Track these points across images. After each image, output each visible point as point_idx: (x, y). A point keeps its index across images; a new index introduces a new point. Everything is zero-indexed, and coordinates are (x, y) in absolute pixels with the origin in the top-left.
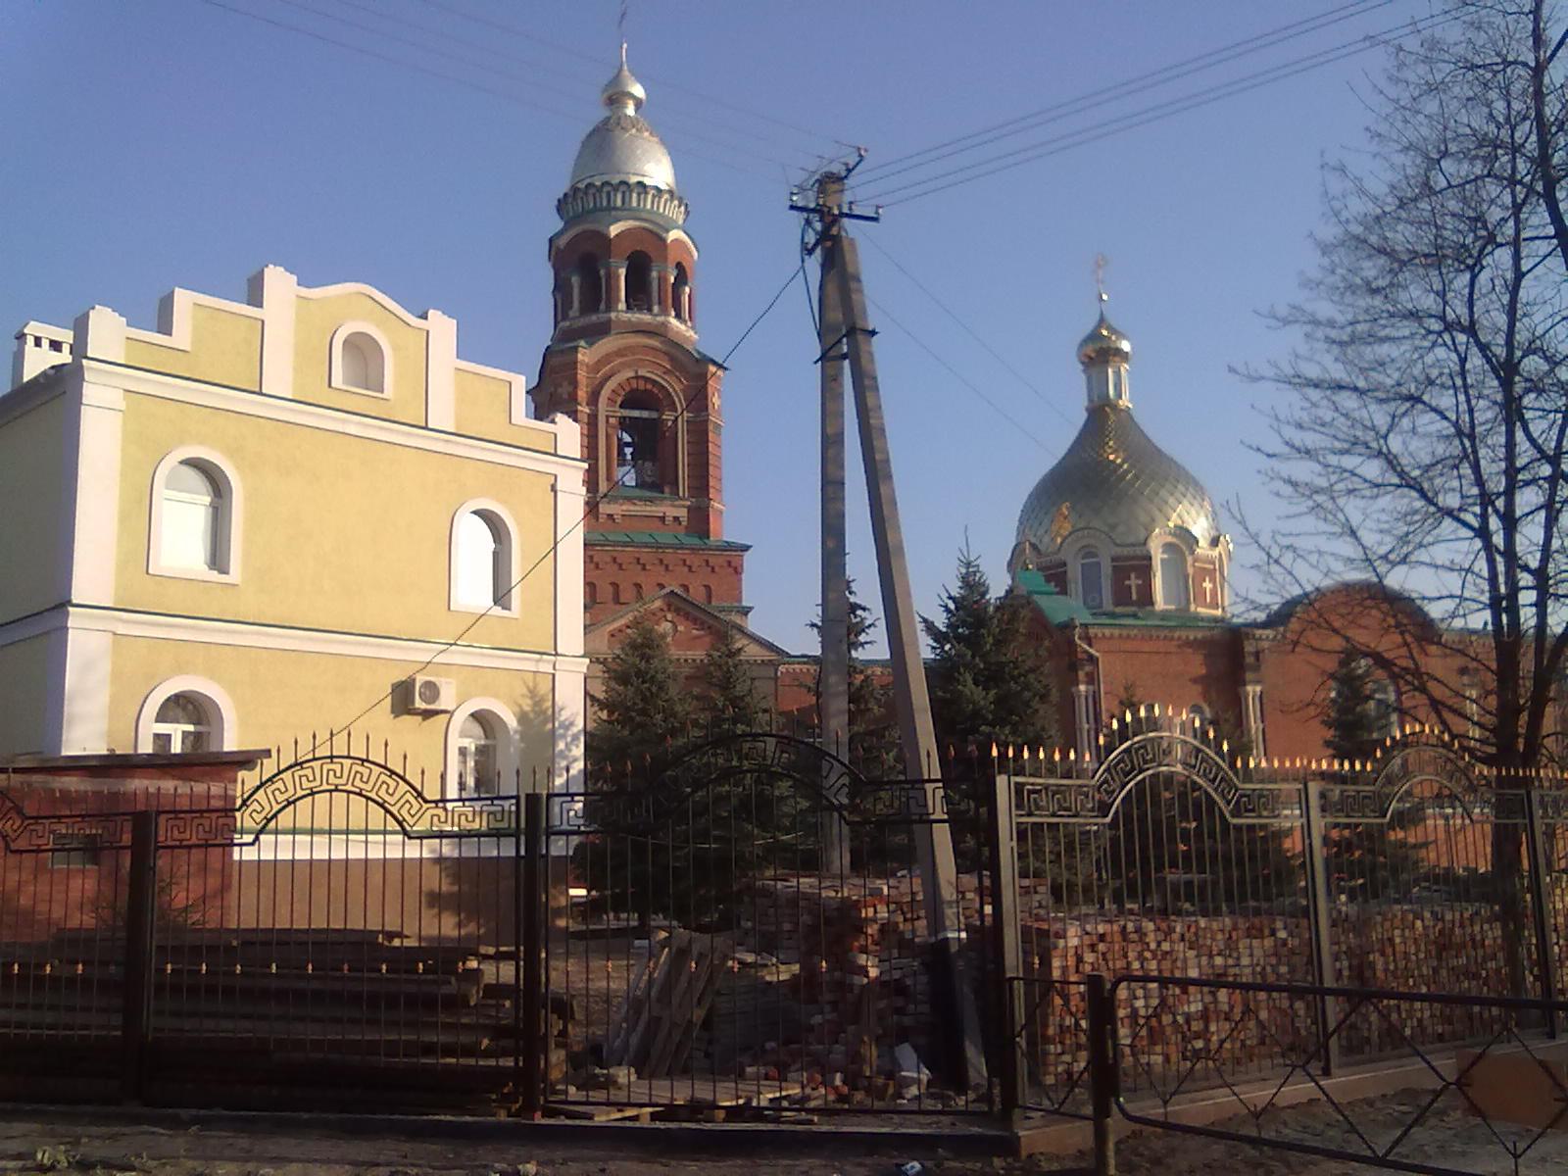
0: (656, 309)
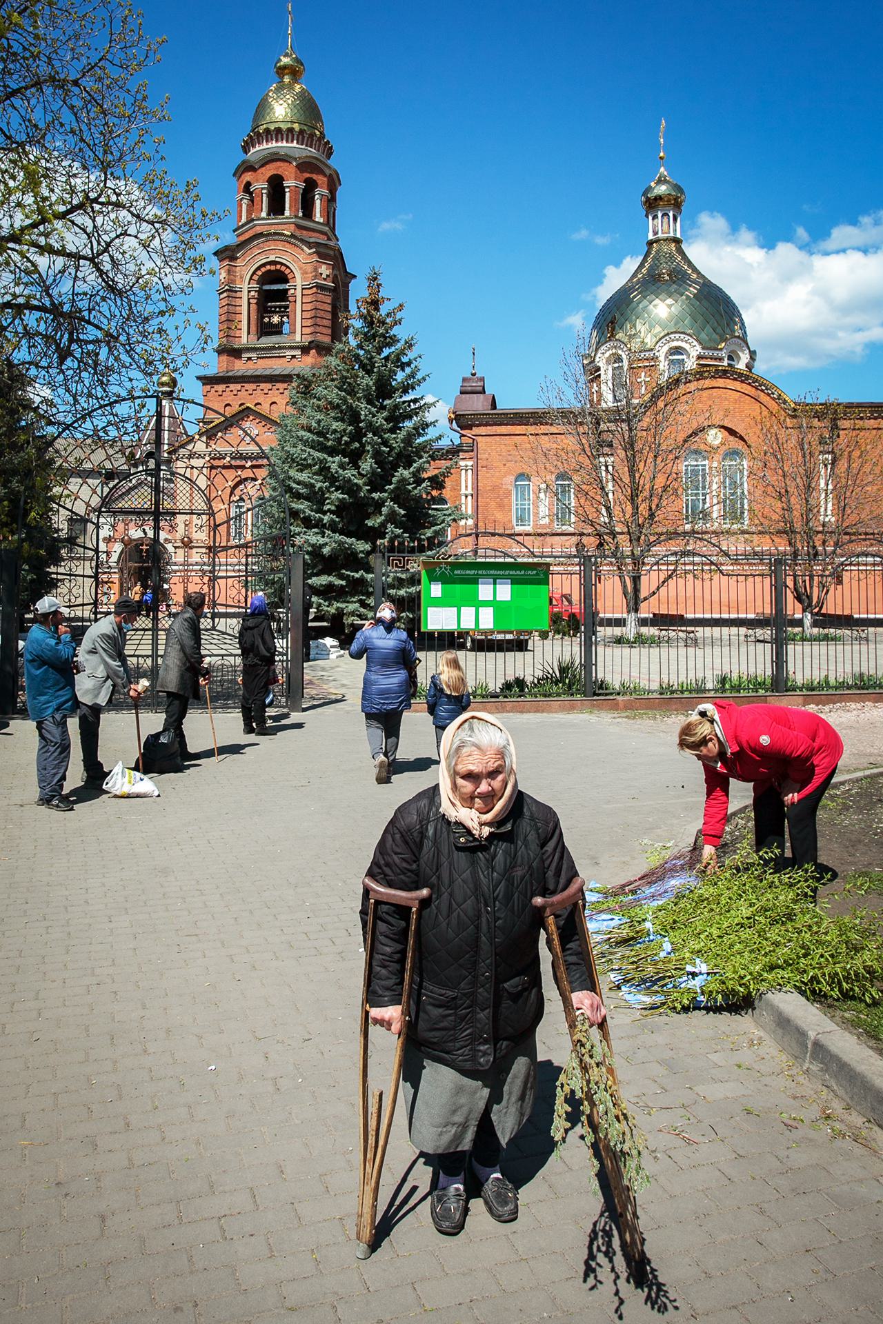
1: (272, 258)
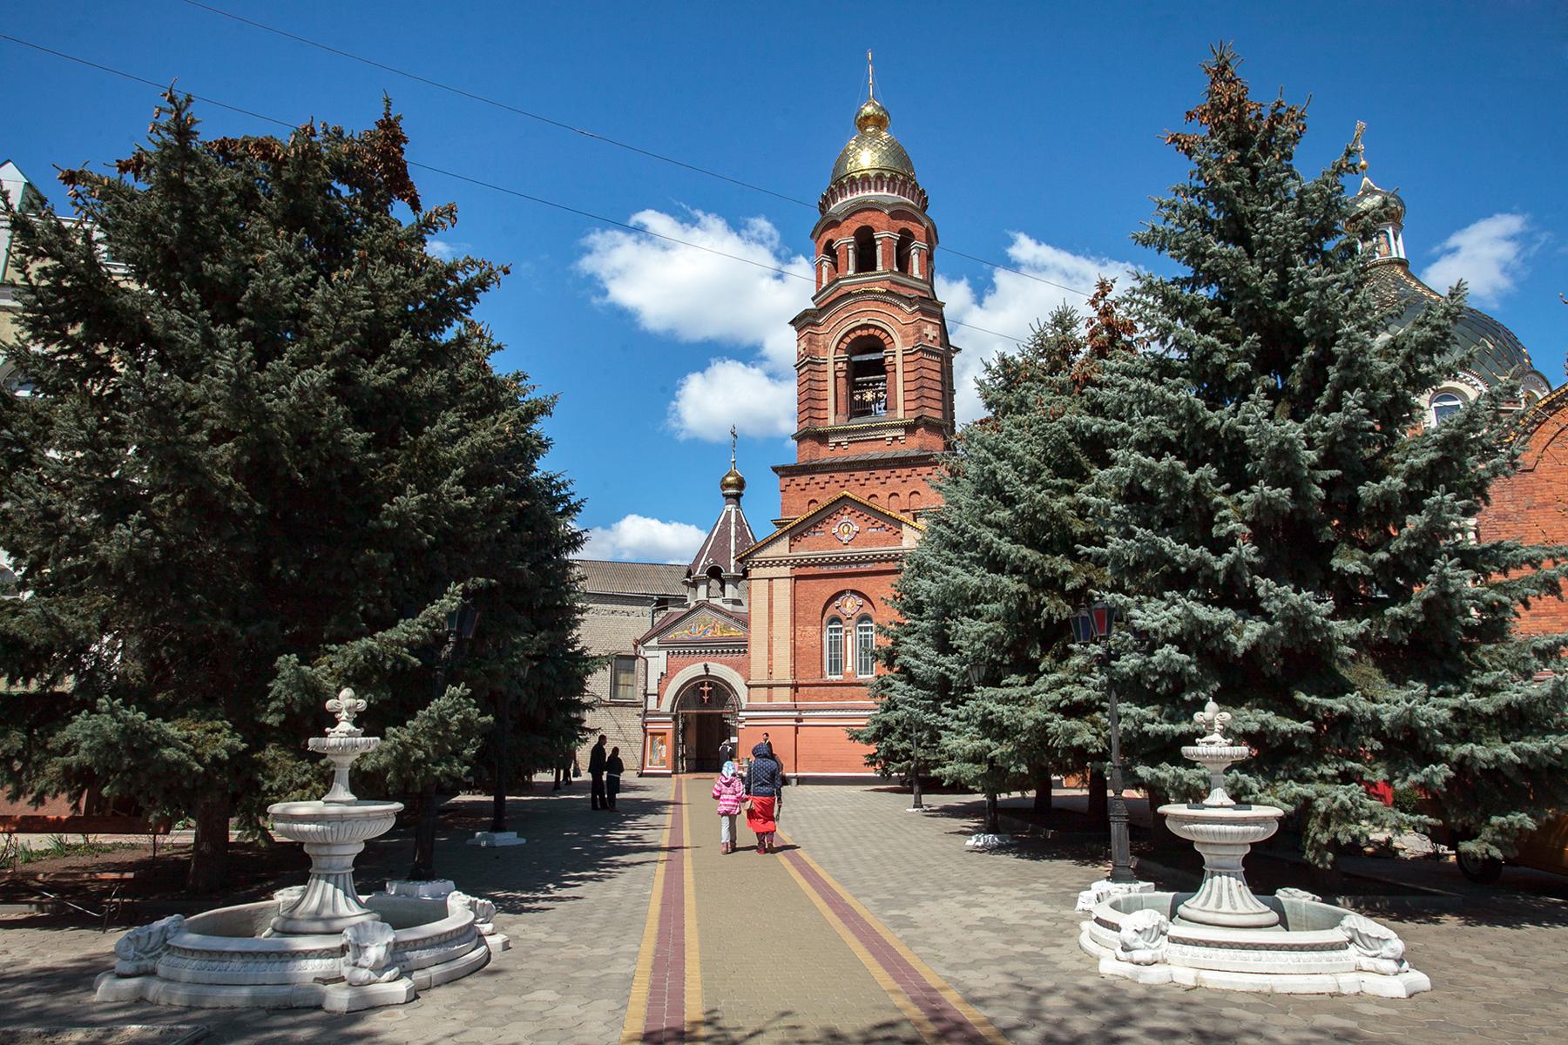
0: (880, 268)
1: (864, 321)
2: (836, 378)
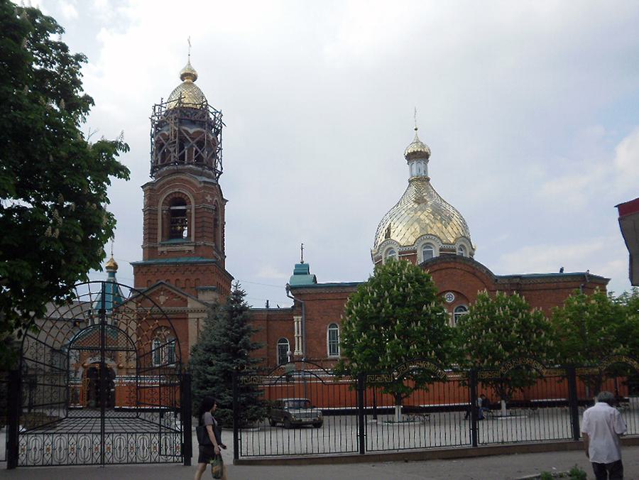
1: (177, 190)
2: (162, 218)
